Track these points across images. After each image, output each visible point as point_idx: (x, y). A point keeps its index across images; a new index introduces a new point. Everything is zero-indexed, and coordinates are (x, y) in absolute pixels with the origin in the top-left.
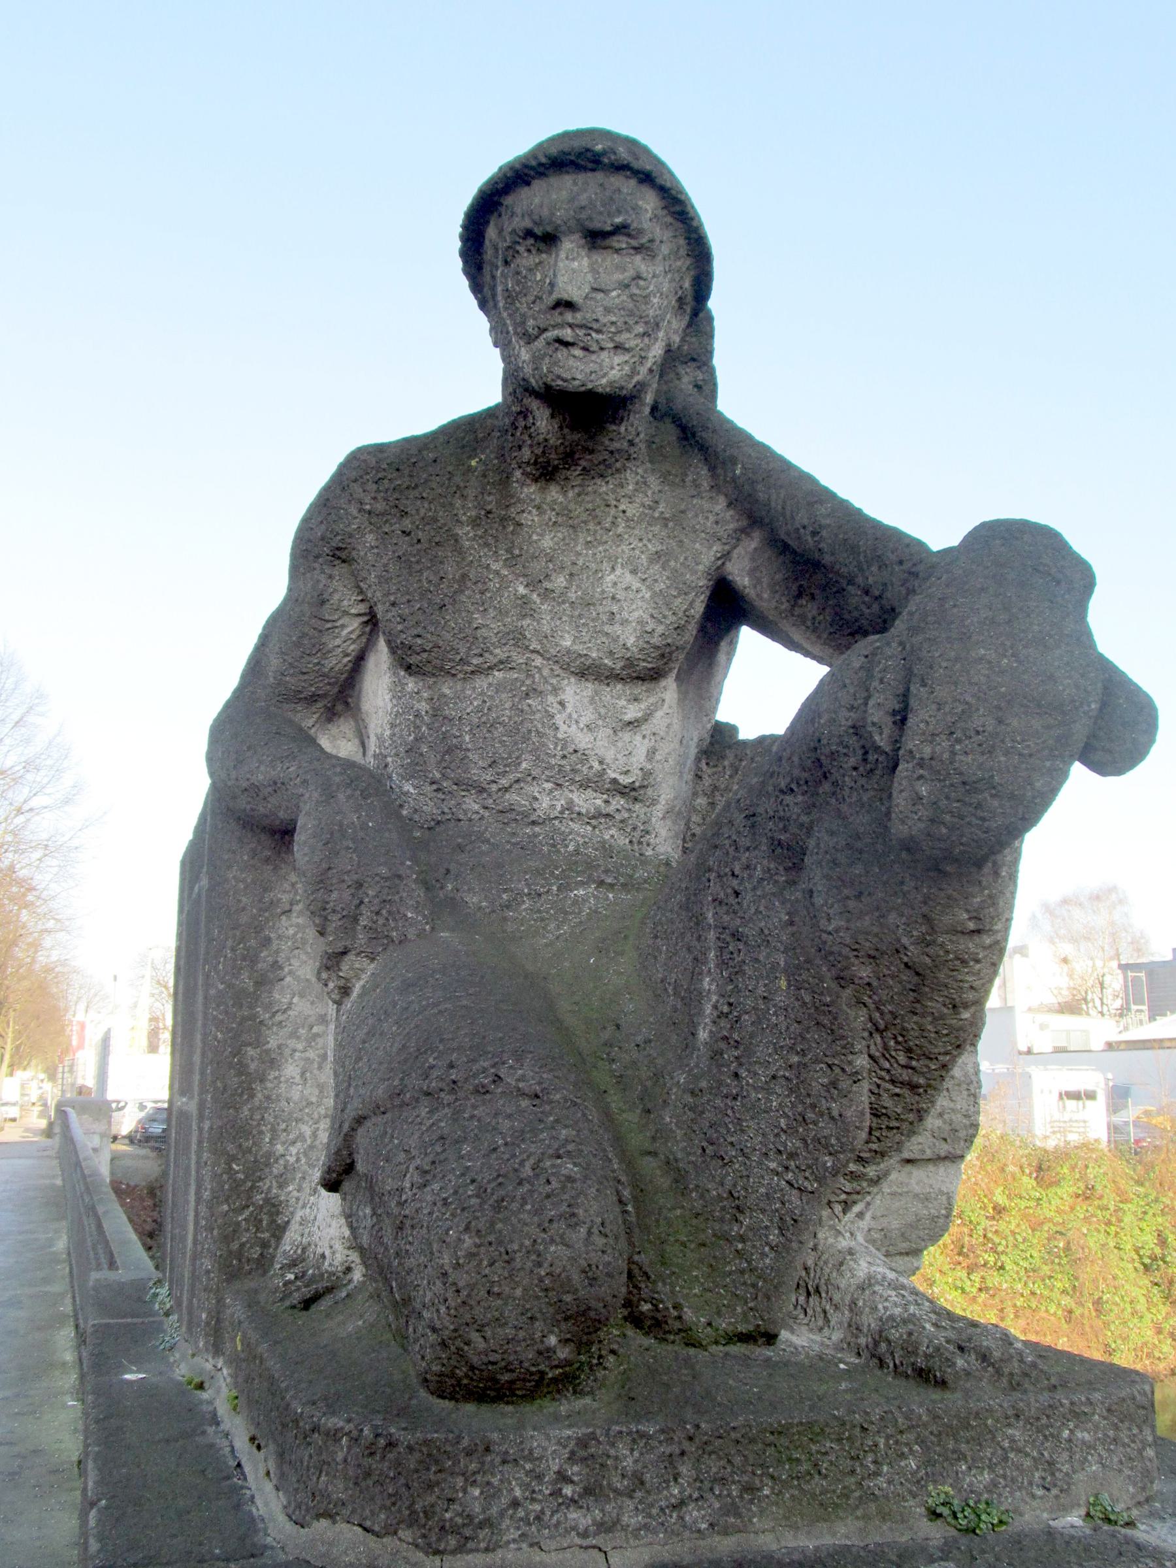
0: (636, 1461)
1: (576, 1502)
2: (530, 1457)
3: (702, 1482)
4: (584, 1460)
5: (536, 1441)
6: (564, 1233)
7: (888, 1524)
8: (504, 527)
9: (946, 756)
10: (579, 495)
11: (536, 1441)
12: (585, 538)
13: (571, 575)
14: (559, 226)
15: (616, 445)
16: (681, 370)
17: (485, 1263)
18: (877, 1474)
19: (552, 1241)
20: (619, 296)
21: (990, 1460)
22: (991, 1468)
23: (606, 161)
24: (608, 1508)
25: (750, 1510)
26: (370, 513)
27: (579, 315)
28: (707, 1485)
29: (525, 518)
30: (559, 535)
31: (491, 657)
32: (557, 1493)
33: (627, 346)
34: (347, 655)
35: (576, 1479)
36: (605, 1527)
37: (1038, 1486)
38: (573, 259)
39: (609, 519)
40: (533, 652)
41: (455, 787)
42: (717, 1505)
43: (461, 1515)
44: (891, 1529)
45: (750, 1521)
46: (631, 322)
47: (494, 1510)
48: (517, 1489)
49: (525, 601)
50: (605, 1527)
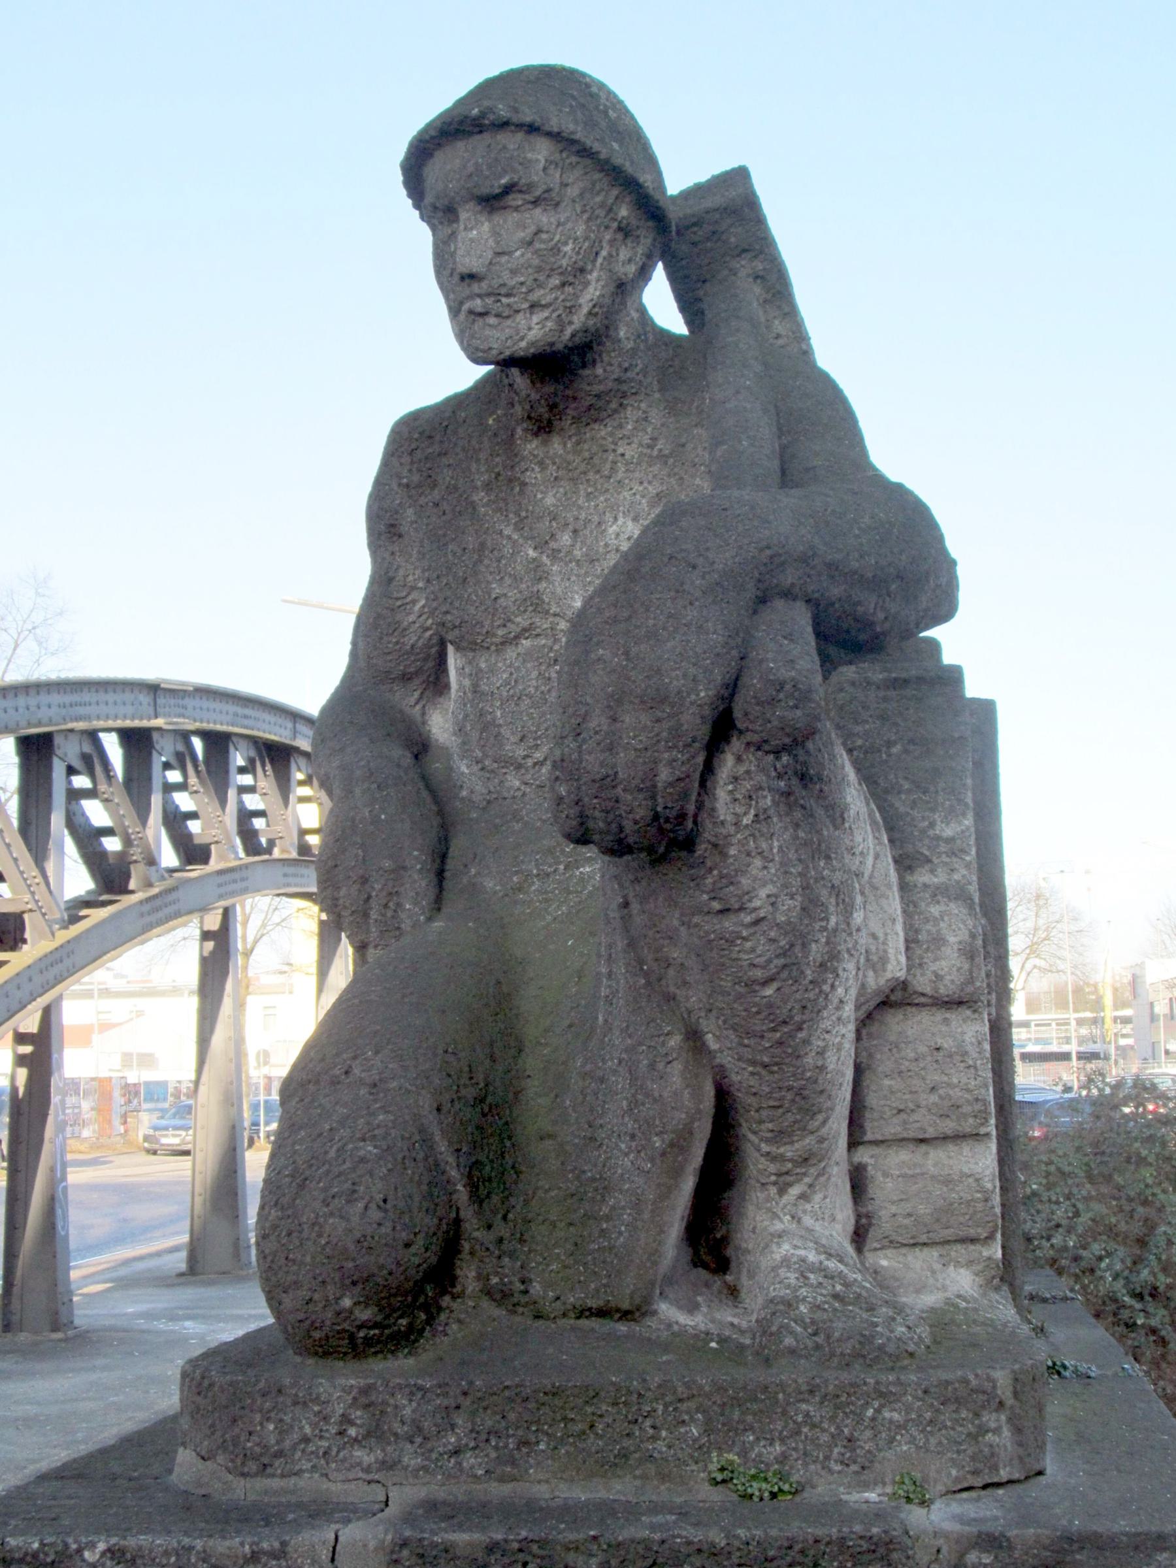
0: (413, 1411)
1: (359, 1442)
2: (317, 1400)
3: (478, 1433)
4: (367, 1406)
5: (323, 1387)
6: (342, 1208)
7: (667, 1485)
8: (512, 489)
9: (575, 756)
10: (578, 443)
11: (323, 1387)
12: (586, 489)
13: (575, 531)
14: (453, 198)
15: (597, 388)
16: (735, 264)
17: (284, 1233)
18: (654, 1438)
19: (332, 1214)
20: (523, 255)
21: (781, 1433)
22: (782, 1440)
23: (487, 122)
24: (389, 1449)
25: (527, 1462)
26: (407, 486)
27: (484, 285)
28: (484, 1436)
29: (529, 477)
30: (561, 490)
31: (513, 626)
32: (341, 1433)
33: (543, 302)
34: (427, 629)
35: (358, 1422)
36: (387, 1465)
37: (836, 1461)
38: (472, 229)
39: (608, 466)
40: (555, 615)
41: (496, 765)
42: (493, 1455)
43: (258, 1445)
44: (669, 1489)
45: (526, 1471)
46: (541, 278)
47: (287, 1444)
48: (307, 1427)
49: (537, 565)
50: (387, 1465)
